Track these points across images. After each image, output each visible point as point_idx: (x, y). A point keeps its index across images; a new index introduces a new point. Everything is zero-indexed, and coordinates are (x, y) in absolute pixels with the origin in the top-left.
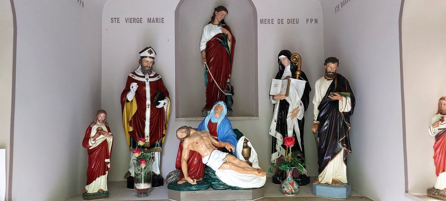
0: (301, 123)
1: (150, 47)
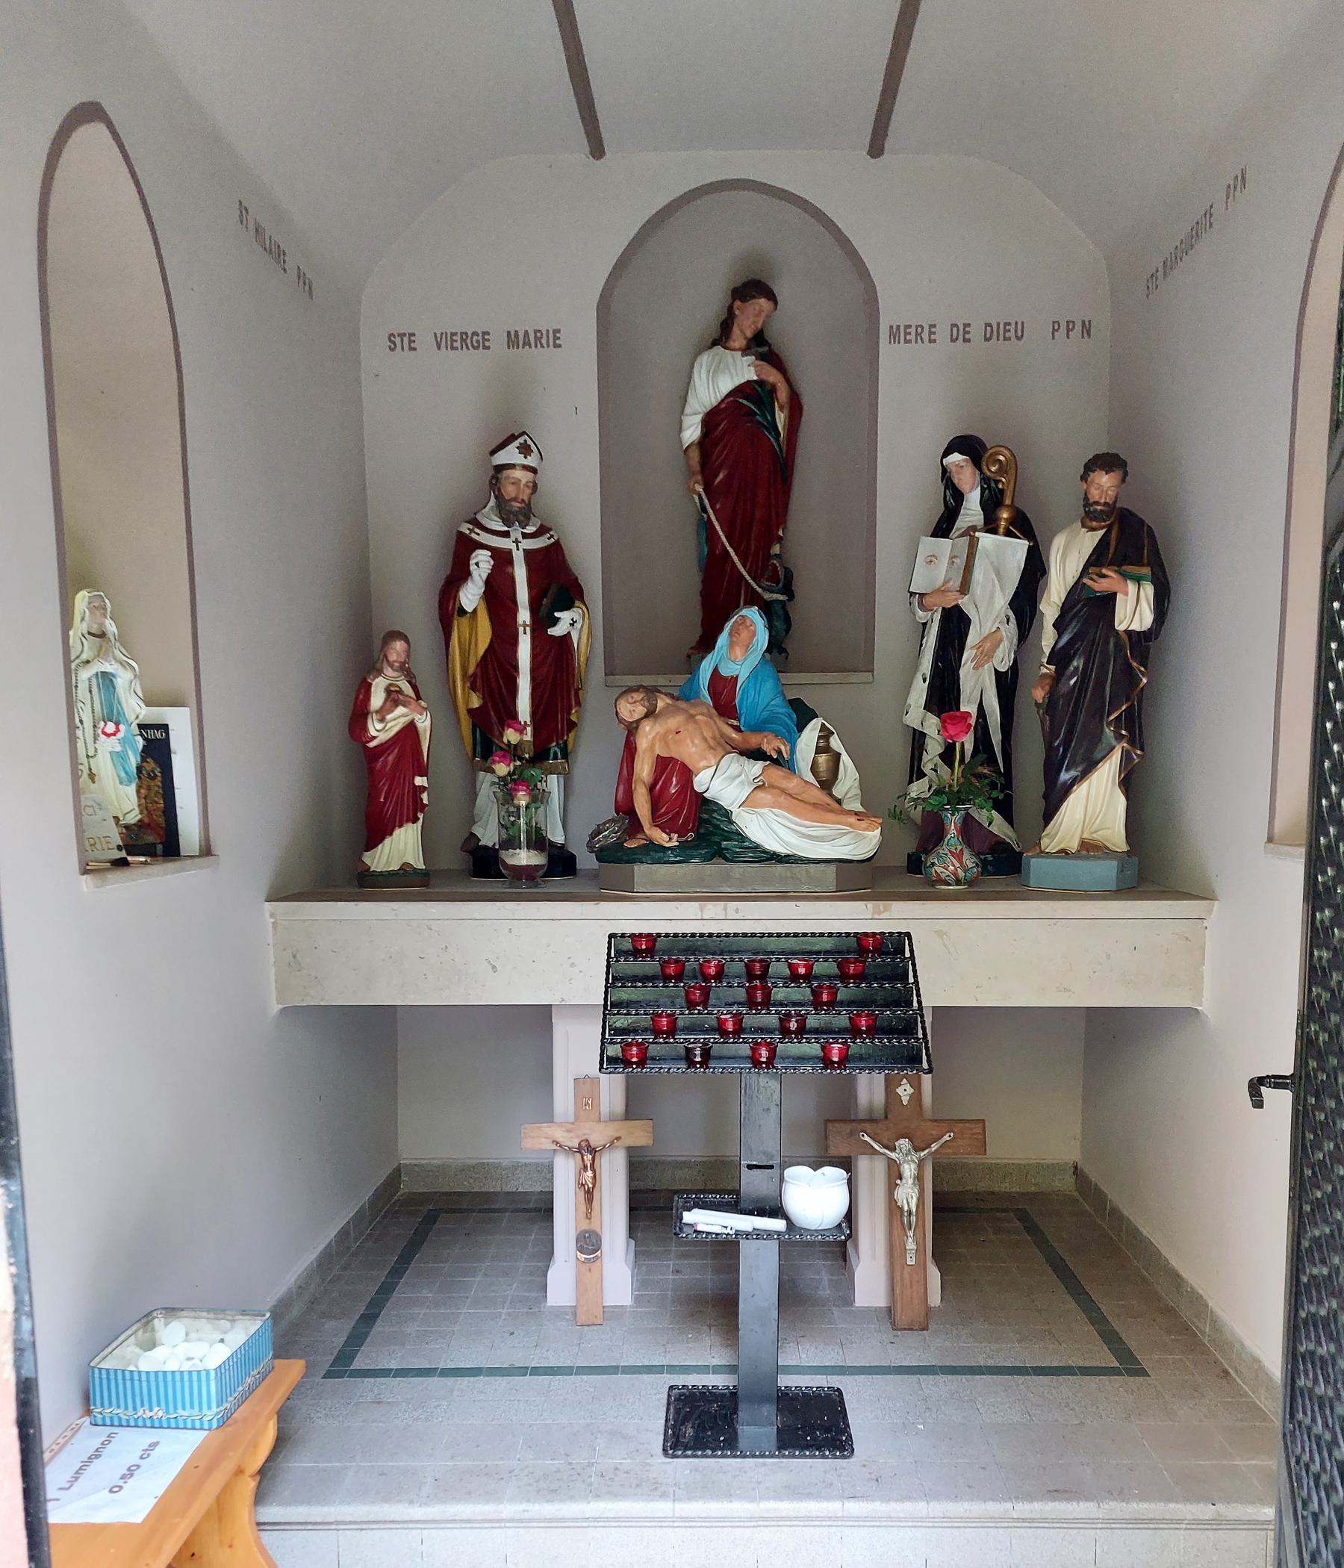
0: (1007, 684)
1: (524, 433)
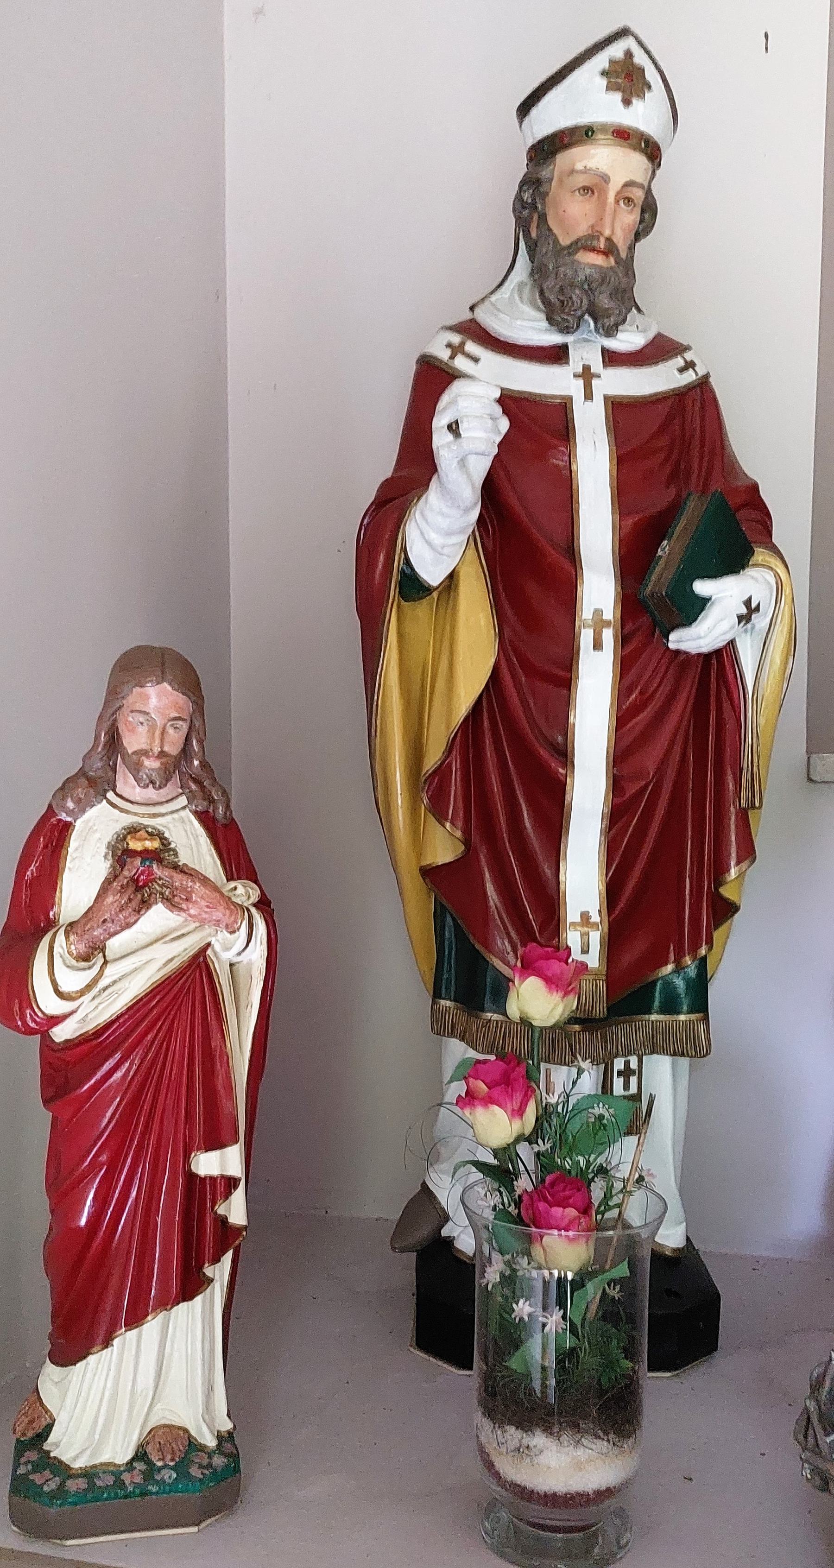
1: (623, 33)
